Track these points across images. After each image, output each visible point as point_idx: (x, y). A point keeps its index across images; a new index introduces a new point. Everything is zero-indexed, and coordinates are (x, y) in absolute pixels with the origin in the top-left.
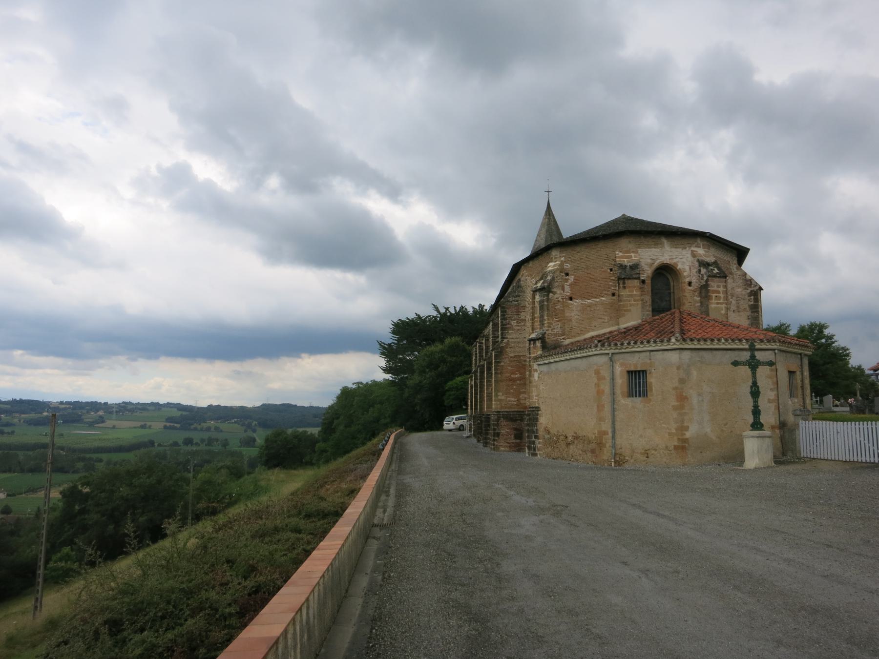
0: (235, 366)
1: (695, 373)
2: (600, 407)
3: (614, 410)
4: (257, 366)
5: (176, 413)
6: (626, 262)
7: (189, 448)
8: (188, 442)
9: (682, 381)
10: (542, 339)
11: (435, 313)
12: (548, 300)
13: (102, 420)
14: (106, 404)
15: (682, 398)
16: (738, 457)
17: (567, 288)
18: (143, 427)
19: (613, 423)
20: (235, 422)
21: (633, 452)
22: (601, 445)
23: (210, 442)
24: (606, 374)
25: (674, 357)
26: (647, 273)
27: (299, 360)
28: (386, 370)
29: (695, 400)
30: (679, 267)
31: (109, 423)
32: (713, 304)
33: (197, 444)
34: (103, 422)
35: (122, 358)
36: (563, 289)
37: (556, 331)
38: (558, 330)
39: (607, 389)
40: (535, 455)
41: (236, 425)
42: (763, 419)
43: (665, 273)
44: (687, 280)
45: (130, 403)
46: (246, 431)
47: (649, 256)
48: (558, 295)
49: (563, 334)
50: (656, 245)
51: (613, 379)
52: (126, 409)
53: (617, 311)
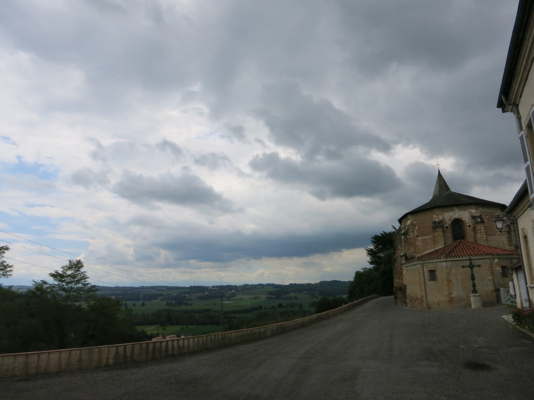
0: (305, 259)
1: (453, 271)
2: (421, 285)
3: (425, 287)
4: (317, 259)
5: (272, 289)
6: (437, 220)
7: (282, 309)
8: (280, 306)
9: (448, 274)
10: (405, 255)
11: (394, 230)
12: (406, 238)
13: (234, 295)
14: (235, 286)
15: (449, 281)
16: (470, 305)
17: (415, 232)
18: (255, 298)
19: (426, 292)
20: (306, 293)
21: (434, 303)
22: (422, 301)
23: (292, 305)
24: (421, 272)
25: (444, 264)
26: (448, 223)
27: (341, 253)
28: (371, 263)
29: (455, 282)
30: (464, 219)
31: (238, 297)
32: (479, 236)
33: (285, 307)
34: (235, 296)
35: (243, 260)
36: (414, 233)
37: (412, 252)
38: (412, 250)
39: (422, 278)
40: (407, 306)
41: (306, 295)
42: (477, 288)
43: (458, 223)
44: (468, 225)
45: (248, 285)
46: (312, 298)
47: (449, 216)
48: (411, 235)
49: (416, 252)
50: (451, 210)
51: (424, 274)
52: (246, 288)
53: (435, 242)
